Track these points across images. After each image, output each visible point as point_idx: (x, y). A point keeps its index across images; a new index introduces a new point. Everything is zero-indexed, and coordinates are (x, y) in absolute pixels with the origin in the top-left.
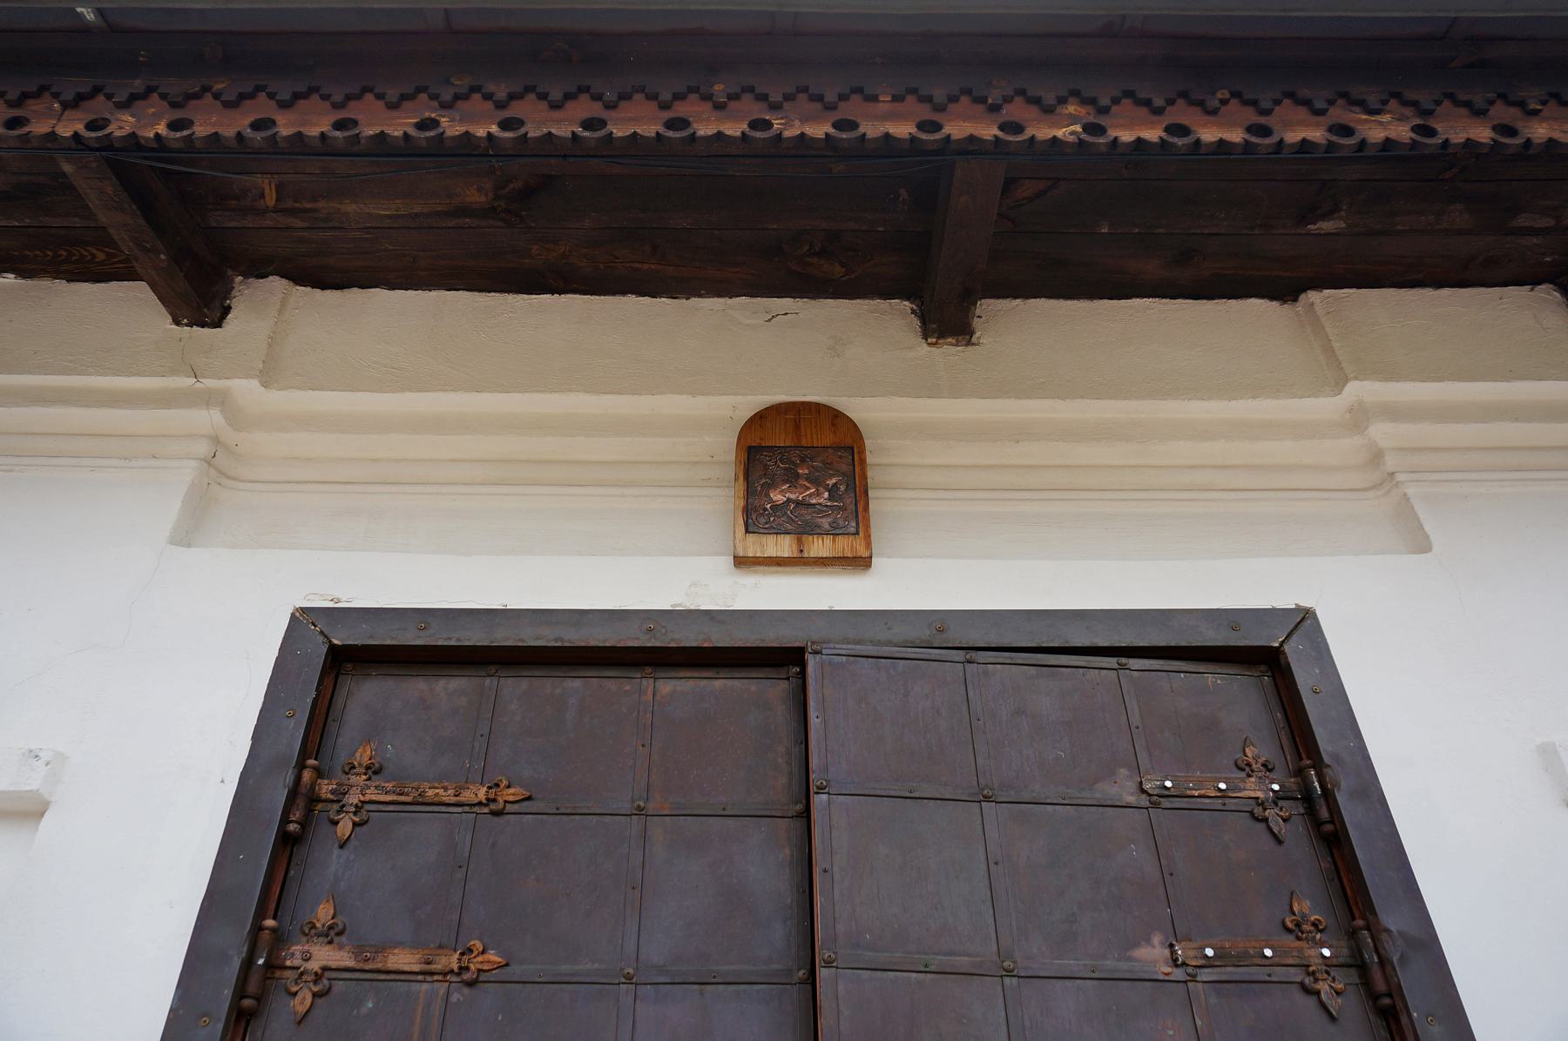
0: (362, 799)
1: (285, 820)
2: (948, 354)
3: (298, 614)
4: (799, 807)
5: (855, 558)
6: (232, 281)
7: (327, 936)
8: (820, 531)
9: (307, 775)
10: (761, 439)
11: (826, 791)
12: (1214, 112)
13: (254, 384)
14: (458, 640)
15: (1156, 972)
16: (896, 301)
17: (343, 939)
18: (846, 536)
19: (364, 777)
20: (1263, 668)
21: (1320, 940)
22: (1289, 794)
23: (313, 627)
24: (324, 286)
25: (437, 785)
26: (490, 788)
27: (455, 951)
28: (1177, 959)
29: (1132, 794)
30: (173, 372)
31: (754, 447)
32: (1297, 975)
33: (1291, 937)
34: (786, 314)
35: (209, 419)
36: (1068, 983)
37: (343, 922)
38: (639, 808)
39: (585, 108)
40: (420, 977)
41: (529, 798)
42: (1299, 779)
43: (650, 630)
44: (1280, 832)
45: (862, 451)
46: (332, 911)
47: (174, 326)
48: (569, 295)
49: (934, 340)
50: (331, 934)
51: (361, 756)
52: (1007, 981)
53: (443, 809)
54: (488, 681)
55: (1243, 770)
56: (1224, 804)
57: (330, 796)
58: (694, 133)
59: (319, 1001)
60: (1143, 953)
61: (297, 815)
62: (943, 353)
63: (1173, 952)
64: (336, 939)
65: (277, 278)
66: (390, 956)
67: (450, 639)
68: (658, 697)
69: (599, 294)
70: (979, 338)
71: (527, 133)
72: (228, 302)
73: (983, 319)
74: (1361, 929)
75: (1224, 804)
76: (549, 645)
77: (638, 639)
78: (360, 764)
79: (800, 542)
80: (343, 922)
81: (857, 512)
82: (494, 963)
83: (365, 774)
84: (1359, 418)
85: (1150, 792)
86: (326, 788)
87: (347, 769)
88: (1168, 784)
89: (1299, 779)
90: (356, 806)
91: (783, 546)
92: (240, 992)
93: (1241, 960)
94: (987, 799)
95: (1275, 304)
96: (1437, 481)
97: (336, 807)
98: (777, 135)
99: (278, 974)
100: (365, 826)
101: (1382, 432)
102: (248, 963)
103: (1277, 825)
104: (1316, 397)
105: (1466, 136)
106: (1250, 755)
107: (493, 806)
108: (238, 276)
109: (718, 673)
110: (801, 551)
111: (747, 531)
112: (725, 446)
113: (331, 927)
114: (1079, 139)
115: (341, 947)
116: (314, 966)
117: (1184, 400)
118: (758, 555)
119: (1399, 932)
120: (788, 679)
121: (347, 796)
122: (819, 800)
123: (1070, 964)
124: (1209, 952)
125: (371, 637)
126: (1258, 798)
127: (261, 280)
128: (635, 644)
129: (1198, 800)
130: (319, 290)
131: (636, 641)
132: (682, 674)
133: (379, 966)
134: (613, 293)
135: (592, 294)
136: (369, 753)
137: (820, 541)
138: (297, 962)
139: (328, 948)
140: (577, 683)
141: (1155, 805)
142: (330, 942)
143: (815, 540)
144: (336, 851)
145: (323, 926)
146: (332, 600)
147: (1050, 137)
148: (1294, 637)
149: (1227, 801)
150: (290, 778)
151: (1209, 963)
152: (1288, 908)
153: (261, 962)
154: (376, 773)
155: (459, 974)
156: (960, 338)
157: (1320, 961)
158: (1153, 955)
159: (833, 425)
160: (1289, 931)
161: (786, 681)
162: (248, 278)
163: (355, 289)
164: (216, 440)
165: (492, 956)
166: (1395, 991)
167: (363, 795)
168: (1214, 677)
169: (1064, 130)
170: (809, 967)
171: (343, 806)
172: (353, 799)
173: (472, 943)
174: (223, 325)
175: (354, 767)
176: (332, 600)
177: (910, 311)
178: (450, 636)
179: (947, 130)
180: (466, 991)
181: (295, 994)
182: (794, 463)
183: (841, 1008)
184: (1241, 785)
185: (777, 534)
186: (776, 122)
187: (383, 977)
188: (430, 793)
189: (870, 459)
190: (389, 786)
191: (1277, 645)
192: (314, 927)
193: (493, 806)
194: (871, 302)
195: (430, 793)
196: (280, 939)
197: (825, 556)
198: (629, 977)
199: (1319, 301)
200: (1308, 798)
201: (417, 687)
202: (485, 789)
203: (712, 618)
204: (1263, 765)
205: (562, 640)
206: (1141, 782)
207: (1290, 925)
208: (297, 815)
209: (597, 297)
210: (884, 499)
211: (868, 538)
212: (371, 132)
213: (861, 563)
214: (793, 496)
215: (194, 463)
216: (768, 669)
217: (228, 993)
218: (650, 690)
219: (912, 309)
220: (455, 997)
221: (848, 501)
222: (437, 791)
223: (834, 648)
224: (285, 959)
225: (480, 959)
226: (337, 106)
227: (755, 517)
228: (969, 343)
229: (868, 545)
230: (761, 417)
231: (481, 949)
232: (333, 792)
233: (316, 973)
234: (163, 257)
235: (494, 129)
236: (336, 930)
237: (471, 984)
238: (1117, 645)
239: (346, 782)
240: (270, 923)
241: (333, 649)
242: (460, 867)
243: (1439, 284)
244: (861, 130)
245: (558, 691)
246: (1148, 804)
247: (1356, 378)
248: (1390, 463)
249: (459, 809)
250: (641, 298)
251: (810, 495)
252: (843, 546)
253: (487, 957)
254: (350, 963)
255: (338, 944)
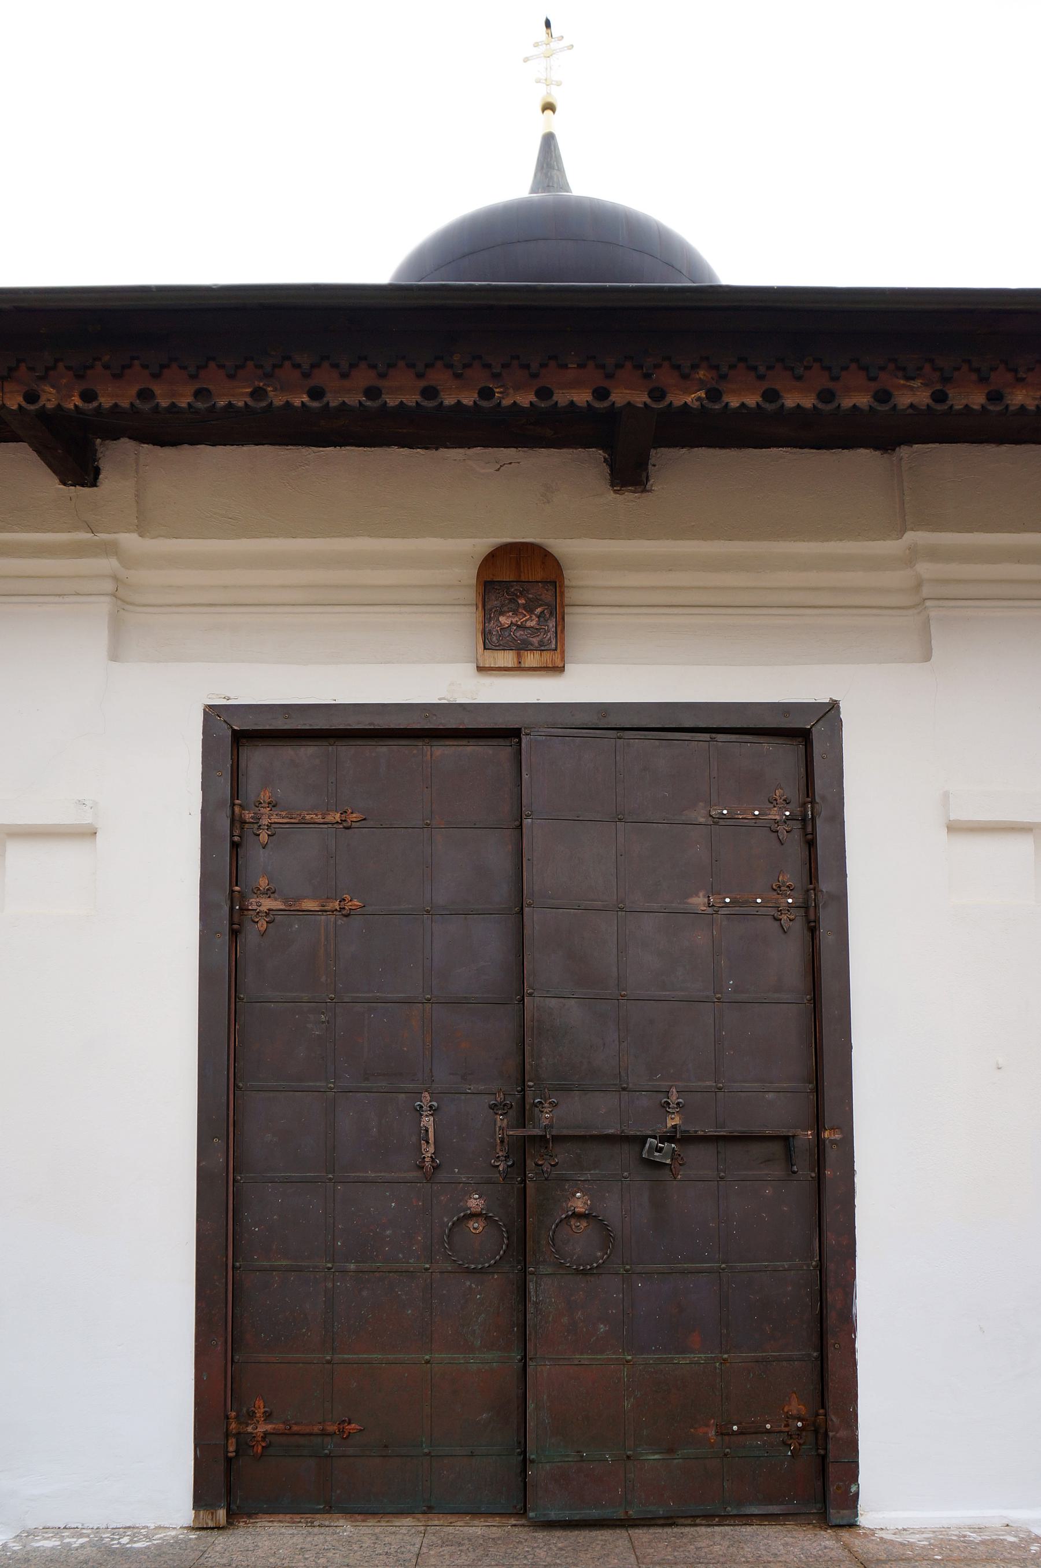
0: (270, 821)
1: (232, 835)
2: (627, 501)
3: (207, 710)
4: (517, 823)
5: (554, 667)
6: (94, 444)
7: (267, 894)
8: (532, 648)
9: (237, 809)
10: (493, 575)
11: (531, 817)
12: (799, 378)
13: (134, 536)
14: (311, 725)
15: (698, 910)
16: (593, 450)
17: (276, 895)
18: (549, 652)
19: (268, 809)
20: (800, 739)
21: (789, 895)
22: (794, 817)
23: (219, 718)
24: (162, 444)
25: (311, 813)
26: (341, 814)
27: (337, 901)
28: (709, 904)
29: (704, 817)
30: (75, 528)
31: (488, 582)
32: (773, 912)
33: (775, 893)
34: (510, 463)
35: (108, 564)
36: (651, 914)
37: (274, 887)
38: (427, 824)
39: (364, 377)
40: (320, 913)
41: (364, 819)
42: (803, 809)
43: (427, 717)
44: (783, 838)
45: (562, 585)
46: (267, 882)
47: (62, 486)
48: (348, 448)
49: (619, 488)
50: (269, 893)
51: (264, 797)
52: (620, 913)
53: (317, 826)
54: (330, 748)
55: (772, 803)
56: (755, 823)
57: (251, 820)
58: (442, 402)
59: (270, 925)
60: (694, 900)
61: (237, 832)
62: (625, 499)
63: (709, 900)
64: (272, 895)
65: (126, 440)
66: (303, 903)
67: (305, 724)
68: (434, 758)
69: (370, 446)
70: (652, 485)
71: (328, 403)
72: (96, 463)
73: (657, 467)
74: (811, 890)
75: (755, 823)
76: (366, 727)
77: (419, 723)
78: (264, 801)
79: (519, 656)
80: (274, 887)
81: (556, 633)
82: (357, 905)
83: (268, 807)
84: (912, 557)
85: (714, 816)
86: (248, 816)
87: (257, 805)
88: (725, 812)
89: (803, 809)
90: (268, 826)
91: (506, 658)
92: (232, 923)
93: (745, 903)
94: (620, 820)
95: (878, 453)
96: (952, 607)
97: (256, 826)
98: (498, 403)
99: (246, 913)
100: (274, 836)
101: (925, 569)
102: (232, 908)
103: (783, 835)
104: (884, 540)
105: (965, 402)
106: (777, 795)
107: (345, 824)
108: (97, 438)
109: (469, 742)
110: (520, 662)
111: (485, 648)
112: (469, 575)
113: (268, 890)
114: (702, 405)
115: (276, 899)
116: (264, 909)
117: (790, 541)
118: (492, 666)
119: (827, 892)
120: (511, 746)
121: (261, 820)
122: (527, 822)
123: (655, 906)
124: (728, 900)
125: (256, 724)
126: (776, 819)
127: (115, 442)
128: (418, 727)
129: (742, 820)
130: (159, 447)
131: (419, 725)
132: (447, 743)
133: (298, 908)
134: (380, 445)
135: (364, 446)
136: (268, 794)
137: (532, 655)
138: (255, 907)
139: (269, 900)
140: (384, 749)
141: (716, 823)
142: (269, 897)
143: (529, 654)
144: (262, 851)
145: (264, 889)
146: (225, 698)
147: (682, 403)
148: (821, 723)
149: (758, 821)
150: (229, 813)
151: (727, 905)
152: (777, 878)
153: (237, 907)
154: (274, 806)
155: (340, 911)
156: (637, 487)
157: (786, 905)
158: (699, 901)
159: (543, 563)
160: (775, 890)
161: (510, 747)
162: (105, 440)
163: (186, 446)
164: (115, 578)
165: (356, 902)
166: (817, 920)
167: (270, 819)
168: (768, 746)
169: (693, 396)
170: (521, 906)
171: (260, 826)
172: (265, 821)
173: (345, 896)
174: (98, 484)
175: (261, 803)
176: (225, 698)
177: (603, 459)
178: (305, 723)
179: (613, 397)
180: (345, 919)
181: (258, 922)
182: (517, 596)
183: (535, 926)
184: (768, 812)
185: (504, 650)
186: (497, 390)
187: (301, 913)
188: (308, 817)
189: (566, 582)
190: (284, 814)
191: (809, 727)
192: (259, 889)
193: (345, 824)
194: (575, 451)
195: (308, 817)
196: (243, 896)
197: (535, 666)
198: (428, 911)
199: (907, 455)
200: (804, 820)
201: (288, 752)
202: (339, 815)
203: (464, 709)
204: (784, 800)
205: (374, 725)
206: (710, 810)
207: (774, 887)
208: (237, 832)
209: (369, 449)
210: (578, 614)
211: (563, 652)
212: (222, 403)
213: (557, 669)
214: (514, 620)
215: (107, 599)
216: (500, 740)
217: (226, 922)
218: (429, 753)
219: (605, 458)
220: (339, 922)
221: (551, 625)
222: (312, 816)
223: (538, 731)
224: (248, 906)
225: (350, 904)
226: (193, 377)
227: (490, 641)
228: (644, 491)
229: (563, 659)
230: (493, 556)
231: (350, 899)
232: (252, 818)
233: (266, 912)
234: (60, 451)
235: (305, 398)
236: (271, 891)
237: (346, 916)
238: (711, 726)
239: (259, 812)
240: (237, 888)
241: (234, 731)
242: (332, 857)
243: (1000, 441)
244: (555, 398)
245: (374, 755)
246: (712, 823)
247: (912, 530)
248: (926, 591)
249: (326, 826)
250: (401, 449)
251: (526, 621)
252: (547, 658)
253: (353, 903)
254: (283, 907)
255: (274, 898)
